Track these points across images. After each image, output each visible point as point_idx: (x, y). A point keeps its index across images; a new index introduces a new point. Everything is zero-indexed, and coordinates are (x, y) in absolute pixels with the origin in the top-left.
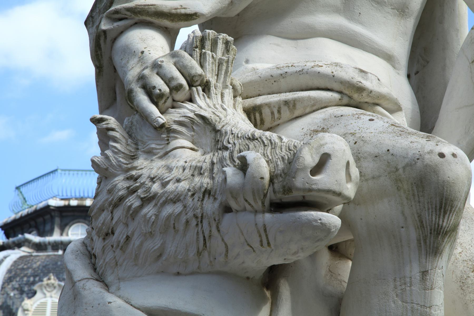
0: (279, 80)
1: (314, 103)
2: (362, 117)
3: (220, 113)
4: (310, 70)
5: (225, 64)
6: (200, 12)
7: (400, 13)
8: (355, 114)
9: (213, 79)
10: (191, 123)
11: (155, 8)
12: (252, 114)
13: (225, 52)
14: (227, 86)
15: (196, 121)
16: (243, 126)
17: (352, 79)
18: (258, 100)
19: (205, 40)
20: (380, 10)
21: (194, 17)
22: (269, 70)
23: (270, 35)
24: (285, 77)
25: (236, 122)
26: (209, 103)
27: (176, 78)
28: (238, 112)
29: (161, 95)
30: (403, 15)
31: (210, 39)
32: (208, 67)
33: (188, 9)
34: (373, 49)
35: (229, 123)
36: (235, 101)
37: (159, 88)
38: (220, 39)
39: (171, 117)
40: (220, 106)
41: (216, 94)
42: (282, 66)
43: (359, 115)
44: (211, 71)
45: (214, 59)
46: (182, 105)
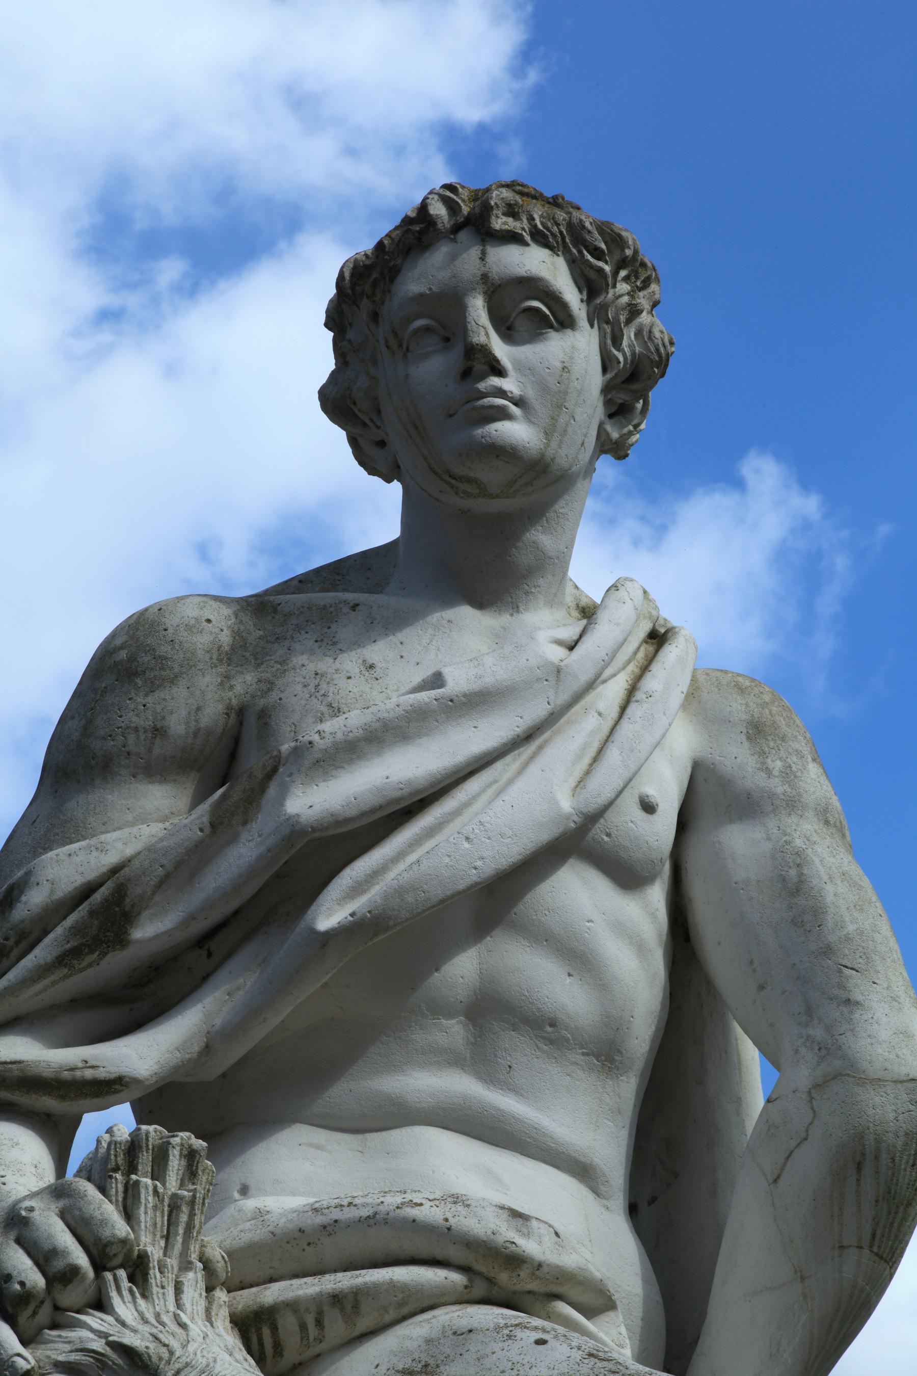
0: (319, 1239)
1: (404, 1297)
2: (519, 1333)
3: (171, 1338)
4: (391, 1214)
5: (185, 1209)
6: (131, 1074)
7: (604, 1064)
8: (501, 1325)
9: (156, 1247)
10: (98, 1367)
11: (21, 1070)
12: (253, 1330)
13: (187, 1177)
14: (191, 1263)
15: (110, 1360)
16: (226, 1369)
17: (492, 1236)
18: (268, 1293)
19: (137, 1151)
20: (556, 1058)
21: (117, 1087)
22: (295, 1215)
23: (301, 1122)
24: (332, 1232)
25: (211, 1360)
26: (145, 1311)
27: (64, 1252)
28: (217, 1331)
29: (26, 1296)
30: (609, 1068)
31: (150, 1147)
32: (143, 1218)
33: (102, 1069)
34: (543, 1150)
35: (193, 1362)
36: (210, 1300)
37: (19, 1279)
38: (173, 1147)
39: (49, 1353)
40: (173, 1318)
41: (163, 1287)
42: (325, 1204)
43: (511, 1329)
44: (151, 1229)
45: (158, 1197)
46: (78, 1319)
